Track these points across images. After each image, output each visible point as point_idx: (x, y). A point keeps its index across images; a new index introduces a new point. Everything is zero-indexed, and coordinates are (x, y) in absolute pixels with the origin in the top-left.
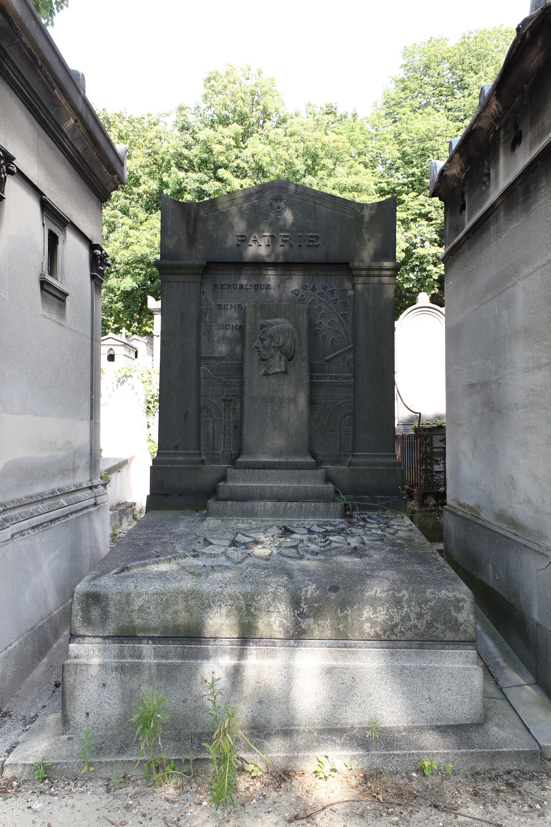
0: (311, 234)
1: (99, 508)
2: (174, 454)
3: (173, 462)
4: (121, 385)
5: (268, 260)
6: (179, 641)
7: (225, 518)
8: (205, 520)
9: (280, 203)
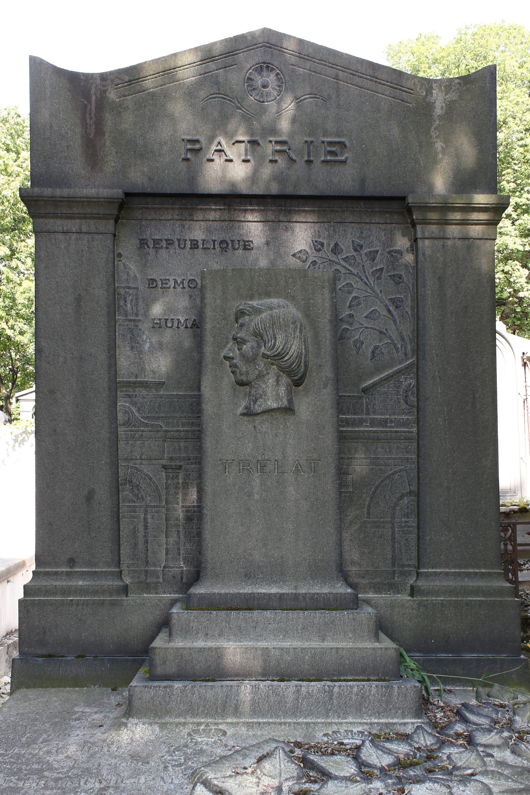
0: (330, 140)
4: (20, 447)
5: (244, 190)
7: (168, 719)
8: (126, 725)
9: (268, 76)
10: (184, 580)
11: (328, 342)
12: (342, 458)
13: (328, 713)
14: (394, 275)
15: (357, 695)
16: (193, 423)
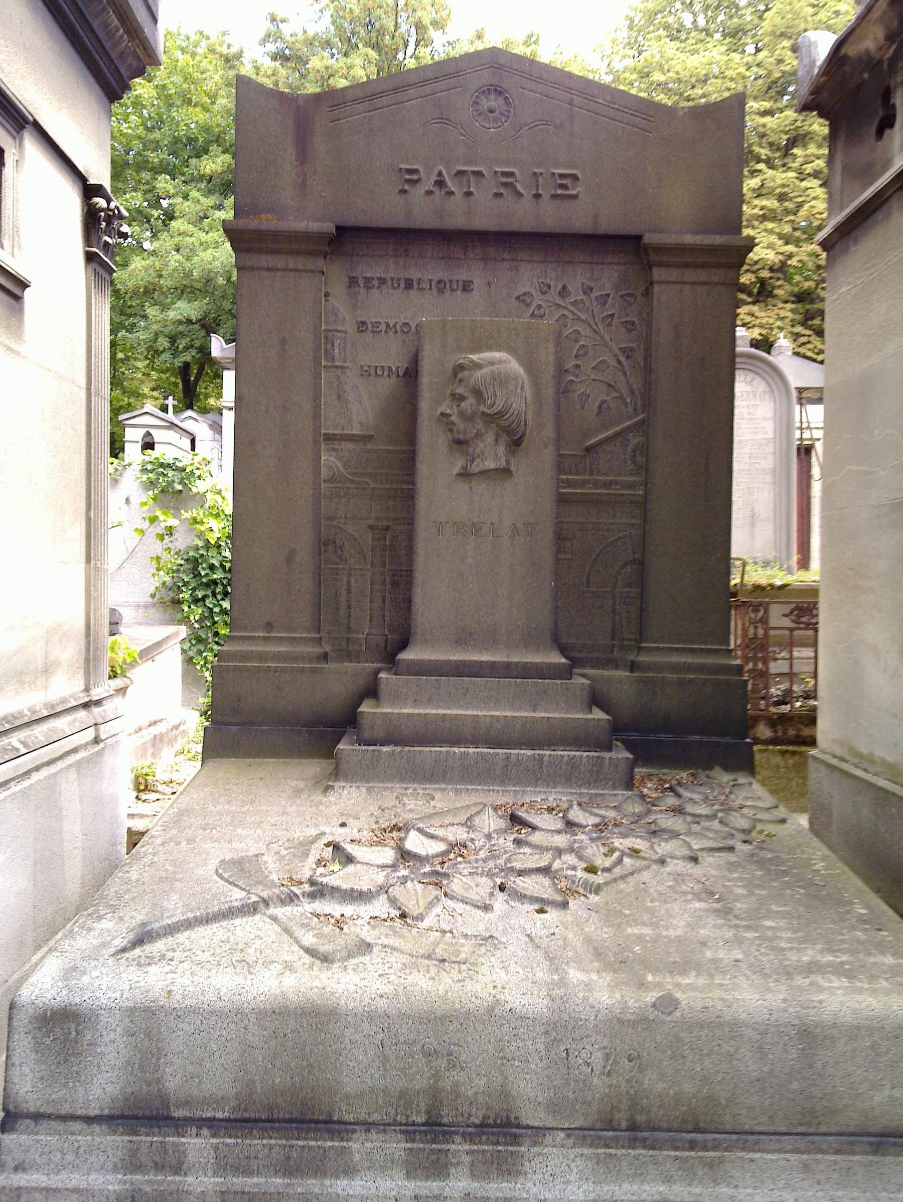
1: (103, 749)
2: (265, 639)
3: (262, 657)
6: (278, 1130)
10: (389, 649)
11: (550, 400)
12: (561, 522)
13: (537, 781)
14: (626, 322)
15: (567, 764)
16: (402, 481)
